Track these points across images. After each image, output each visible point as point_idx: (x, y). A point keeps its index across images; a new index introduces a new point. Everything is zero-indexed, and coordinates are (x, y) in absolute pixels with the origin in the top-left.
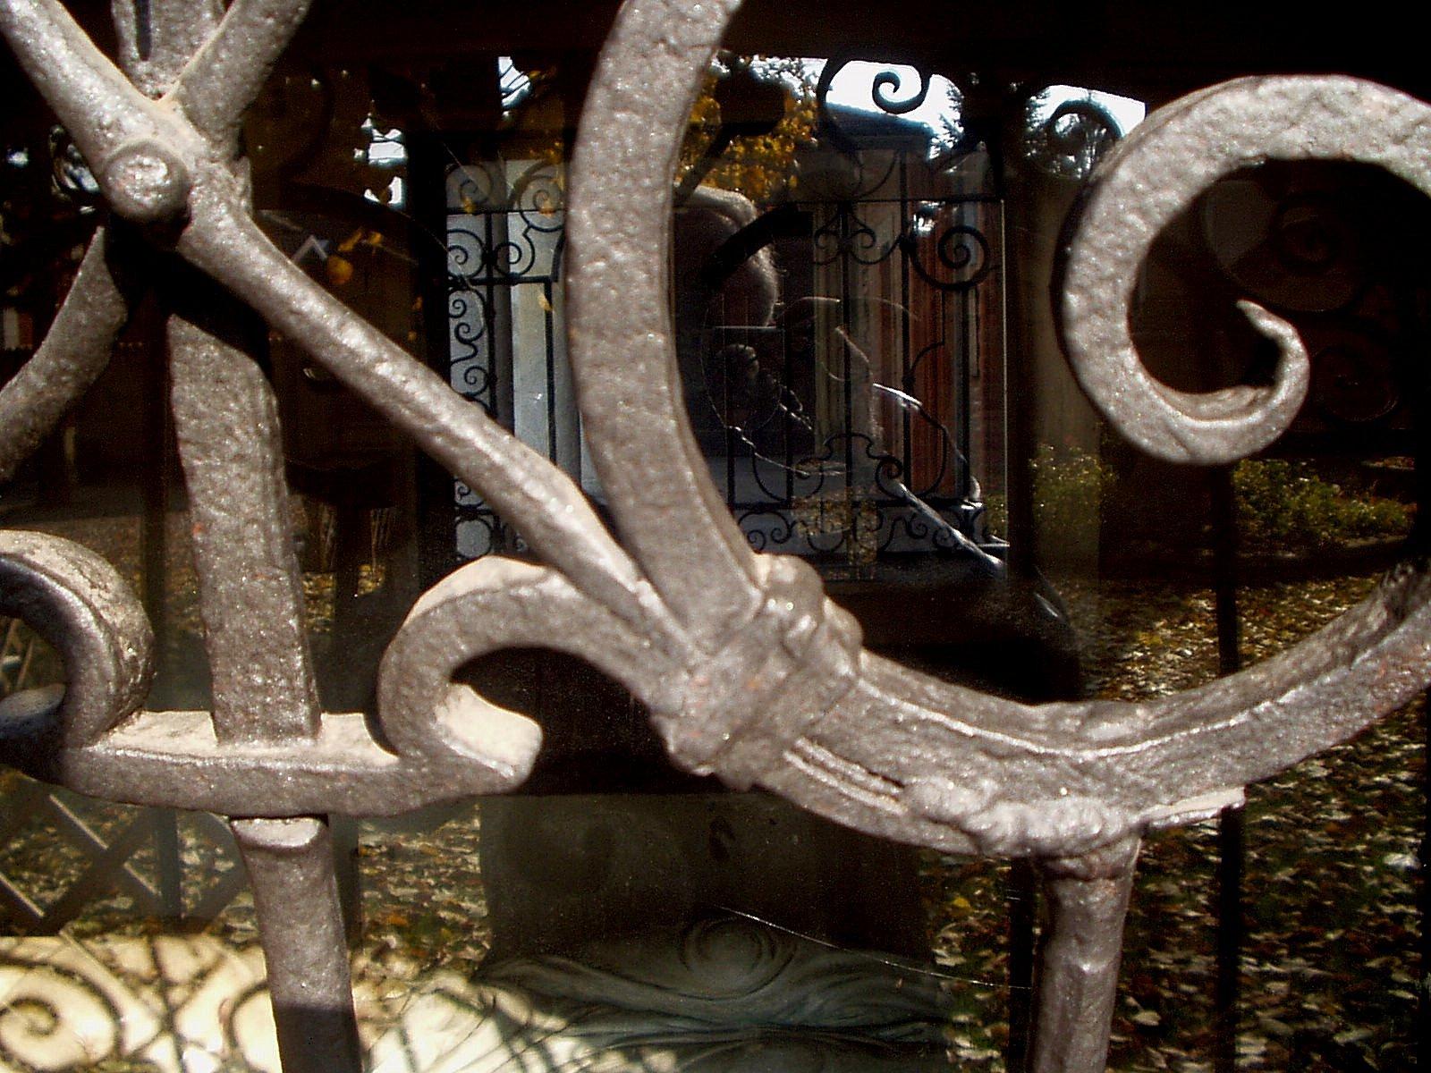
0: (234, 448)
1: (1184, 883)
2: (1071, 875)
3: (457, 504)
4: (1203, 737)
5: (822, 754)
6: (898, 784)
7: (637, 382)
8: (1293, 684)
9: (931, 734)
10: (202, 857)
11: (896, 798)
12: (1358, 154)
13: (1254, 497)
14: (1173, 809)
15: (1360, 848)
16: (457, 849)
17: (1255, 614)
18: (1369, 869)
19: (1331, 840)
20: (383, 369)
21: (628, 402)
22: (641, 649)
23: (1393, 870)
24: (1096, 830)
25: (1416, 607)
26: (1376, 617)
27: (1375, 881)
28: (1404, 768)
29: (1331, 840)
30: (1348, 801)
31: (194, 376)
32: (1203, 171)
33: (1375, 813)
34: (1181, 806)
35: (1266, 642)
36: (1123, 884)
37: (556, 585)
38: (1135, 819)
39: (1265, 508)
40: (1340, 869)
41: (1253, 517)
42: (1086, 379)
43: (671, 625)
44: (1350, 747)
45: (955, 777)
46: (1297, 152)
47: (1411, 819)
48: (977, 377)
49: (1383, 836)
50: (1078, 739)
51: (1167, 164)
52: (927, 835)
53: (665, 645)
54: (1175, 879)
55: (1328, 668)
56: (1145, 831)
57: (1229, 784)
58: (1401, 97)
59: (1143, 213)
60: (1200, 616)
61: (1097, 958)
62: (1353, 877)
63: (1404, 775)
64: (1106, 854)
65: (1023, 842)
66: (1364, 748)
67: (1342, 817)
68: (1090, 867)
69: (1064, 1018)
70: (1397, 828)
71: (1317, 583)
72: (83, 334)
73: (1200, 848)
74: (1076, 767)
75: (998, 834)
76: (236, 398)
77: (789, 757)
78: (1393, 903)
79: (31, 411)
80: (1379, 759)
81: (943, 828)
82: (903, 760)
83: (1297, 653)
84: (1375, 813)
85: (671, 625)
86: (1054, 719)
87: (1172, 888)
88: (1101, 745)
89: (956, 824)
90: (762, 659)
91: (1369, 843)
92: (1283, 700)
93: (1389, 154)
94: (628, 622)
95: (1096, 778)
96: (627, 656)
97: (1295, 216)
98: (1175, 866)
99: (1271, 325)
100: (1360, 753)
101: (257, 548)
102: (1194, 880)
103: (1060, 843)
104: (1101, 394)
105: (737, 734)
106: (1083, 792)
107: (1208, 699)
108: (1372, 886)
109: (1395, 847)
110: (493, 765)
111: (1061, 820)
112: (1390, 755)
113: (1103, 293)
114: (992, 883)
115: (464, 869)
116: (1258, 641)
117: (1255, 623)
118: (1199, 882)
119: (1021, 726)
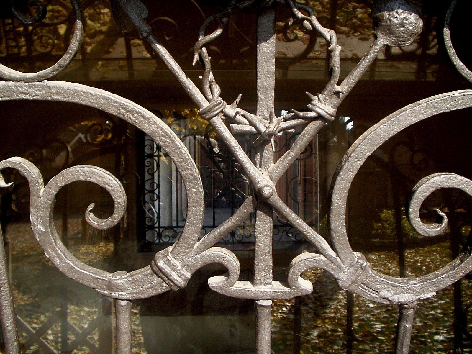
0: (266, 233)
1: (371, 346)
2: (406, 308)
3: (147, 225)
4: (429, 283)
5: (365, 287)
6: (377, 292)
7: (339, 222)
8: (444, 274)
9: (383, 283)
10: (54, 337)
11: (377, 294)
12: (456, 187)
13: (388, 222)
14: (424, 296)
15: (426, 334)
16: (137, 335)
17: (390, 260)
18: (429, 340)
19: (417, 332)
20: (298, 221)
21: (339, 227)
22: (336, 268)
23: (437, 341)
24: (411, 300)
25: (465, 260)
26: (458, 262)
27: (431, 344)
28: (439, 309)
29: (417, 332)
30: (422, 320)
31: (260, 221)
32: (432, 190)
33: (430, 323)
34: (425, 295)
35: (394, 269)
36: (414, 310)
37: (322, 257)
38: (417, 298)
39: (392, 225)
40: (420, 341)
41: (388, 229)
42: (412, 223)
43: (342, 265)
44: (422, 302)
45: (387, 291)
46: (447, 187)
47: (441, 325)
48: (300, 184)
49: (433, 330)
50: (408, 284)
51: (426, 189)
52: (382, 301)
53: (340, 268)
54: (368, 344)
55: (450, 271)
56: (419, 300)
57: (433, 291)
58: (463, 178)
59: (422, 196)
60: (372, 261)
61: (409, 324)
62: (424, 343)
63: (439, 311)
64: (413, 304)
65: (399, 302)
66: (426, 303)
67: (420, 324)
68: (410, 307)
69: (403, 336)
70: (437, 327)
71: (409, 250)
72: (245, 214)
73: (375, 334)
74: (408, 288)
75: (394, 301)
76: (267, 225)
77: (359, 287)
78: (437, 351)
79: (232, 226)
80: (431, 306)
81: (385, 300)
82: (379, 287)
83: (444, 268)
84: (430, 323)
85: (342, 265)
86: (403, 280)
87: (367, 347)
88: (412, 284)
89: (387, 299)
90: (357, 270)
91: (429, 332)
92: (443, 276)
93: (461, 187)
94: (334, 264)
95: (411, 291)
96: (333, 269)
97: (446, 196)
98: (367, 340)
99: (441, 214)
100: (425, 304)
101: (267, 251)
102: (374, 344)
103: (405, 302)
104: (414, 225)
105: (352, 283)
106: (409, 293)
107: (429, 277)
108: (431, 346)
109: (437, 333)
110: (307, 289)
111: (405, 298)
112: (434, 305)
113: (415, 209)
114: (310, 346)
115: (140, 341)
116: (391, 269)
117: (390, 263)
118: (376, 345)
119: (398, 282)
